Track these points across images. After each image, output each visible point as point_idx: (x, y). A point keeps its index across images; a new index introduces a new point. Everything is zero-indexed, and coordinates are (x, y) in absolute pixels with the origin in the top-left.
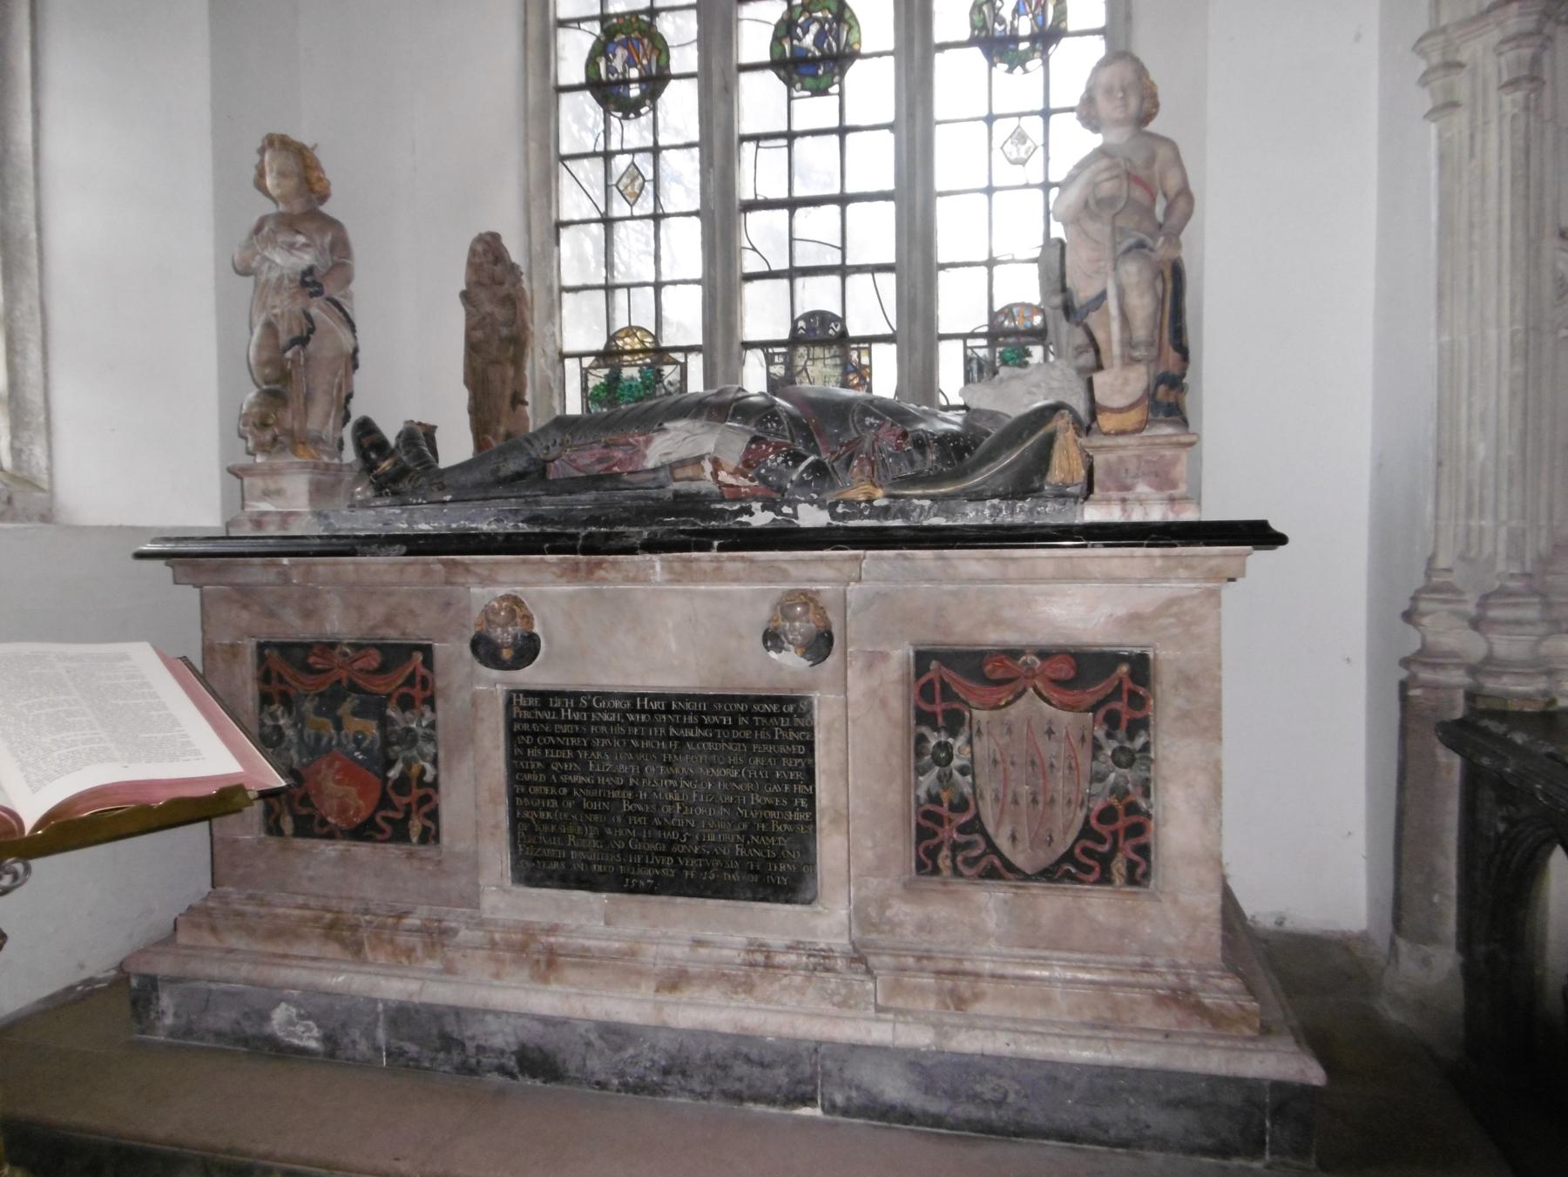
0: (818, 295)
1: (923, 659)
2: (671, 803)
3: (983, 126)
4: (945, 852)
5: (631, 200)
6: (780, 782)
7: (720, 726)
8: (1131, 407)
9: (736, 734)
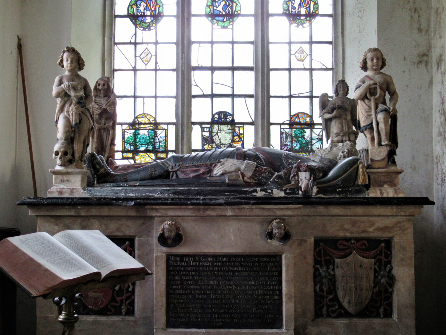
0: (223, 105)
1: (317, 242)
2: (230, 294)
3: (287, 46)
4: (325, 309)
5: (146, 63)
6: (270, 285)
7: (248, 266)
8: (382, 160)
9: (254, 269)
